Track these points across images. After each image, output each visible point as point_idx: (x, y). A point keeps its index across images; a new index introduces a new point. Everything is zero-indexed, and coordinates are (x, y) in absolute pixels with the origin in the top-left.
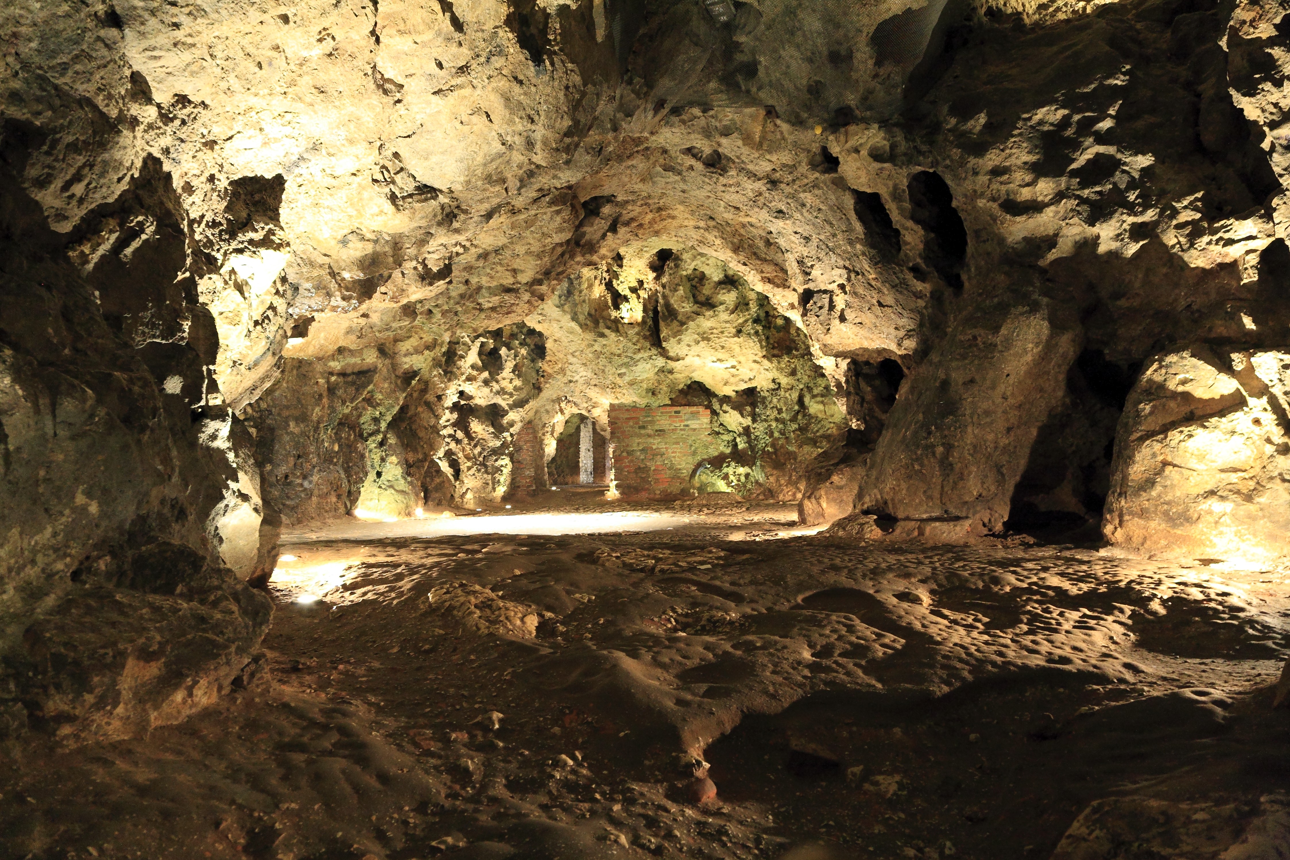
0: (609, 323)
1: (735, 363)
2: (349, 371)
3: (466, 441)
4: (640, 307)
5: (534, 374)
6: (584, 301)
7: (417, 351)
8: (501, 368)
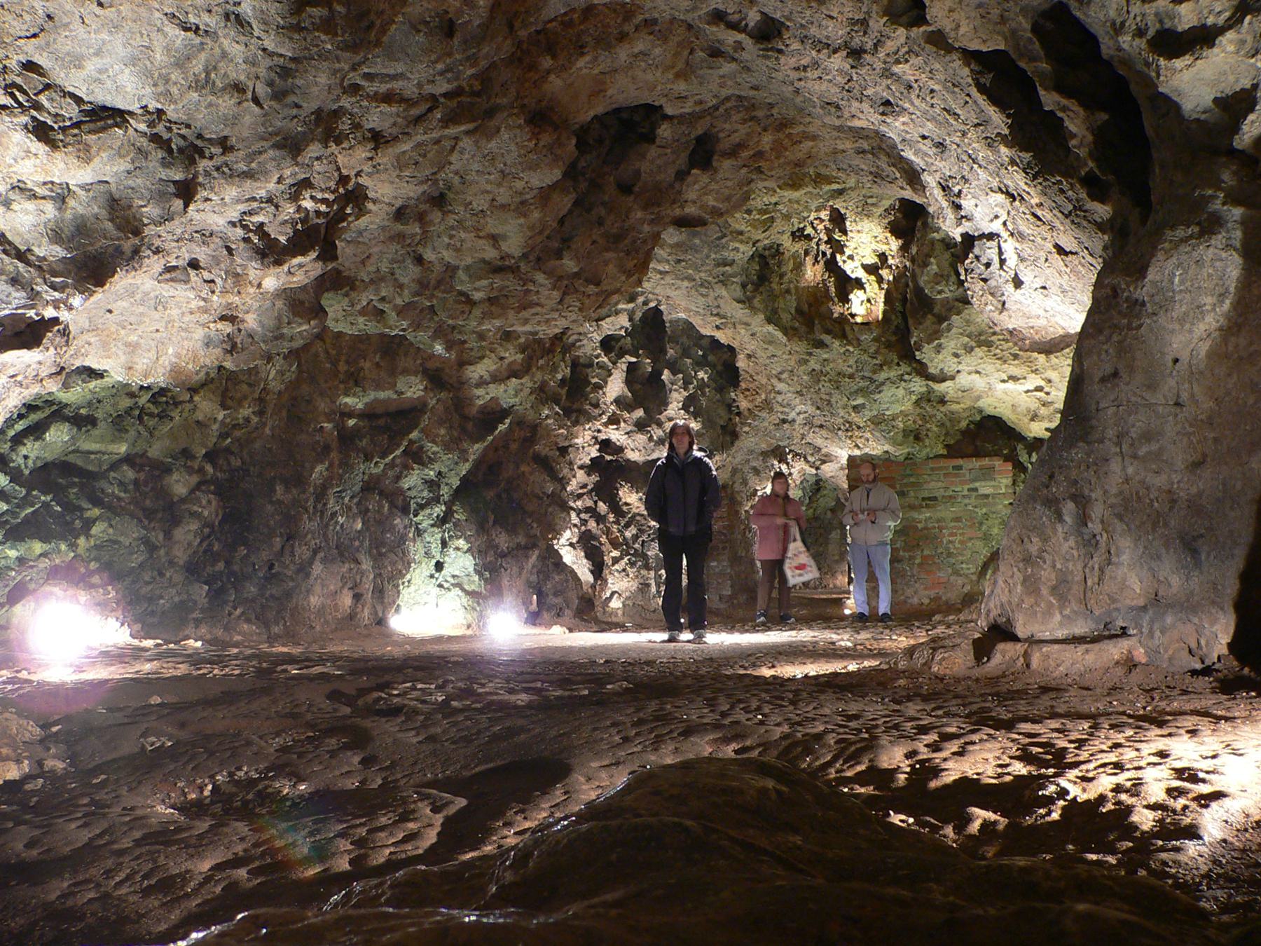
0: (829, 325)
1: (1043, 383)
2: (379, 411)
3: (611, 517)
4: (881, 298)
5: (722, 412)
6: (788, 291)
7: (496, 378)
8: (665, 404)
